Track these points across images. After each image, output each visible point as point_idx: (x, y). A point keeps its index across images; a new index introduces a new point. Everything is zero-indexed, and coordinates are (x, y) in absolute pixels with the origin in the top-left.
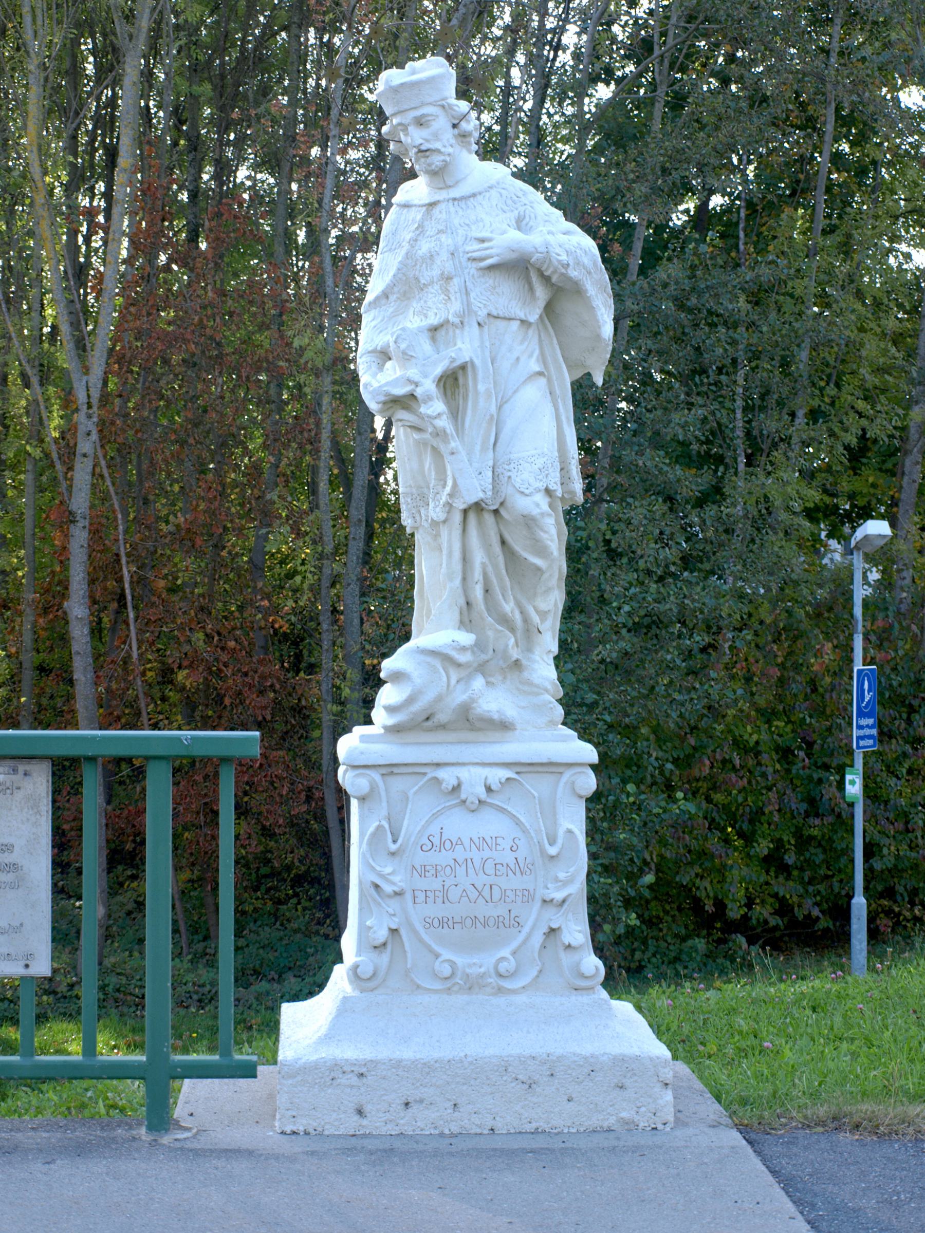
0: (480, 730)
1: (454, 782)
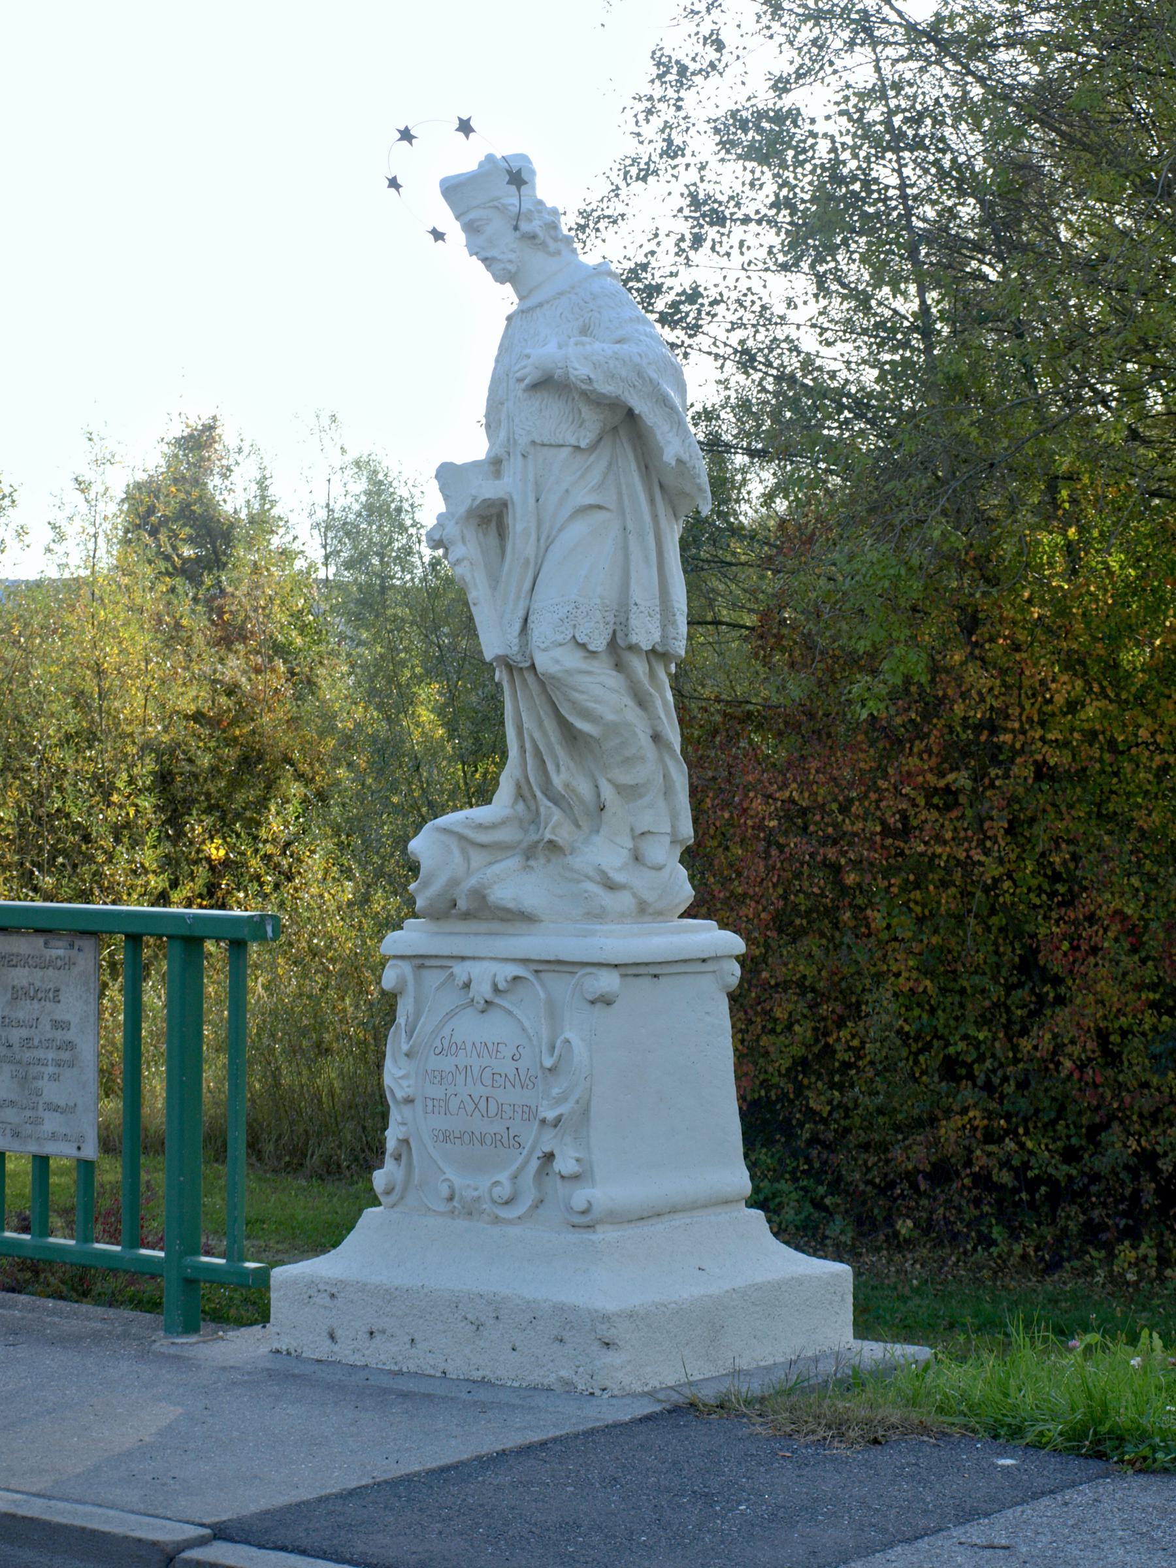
0: (508, 920)
1: (465, 978)
